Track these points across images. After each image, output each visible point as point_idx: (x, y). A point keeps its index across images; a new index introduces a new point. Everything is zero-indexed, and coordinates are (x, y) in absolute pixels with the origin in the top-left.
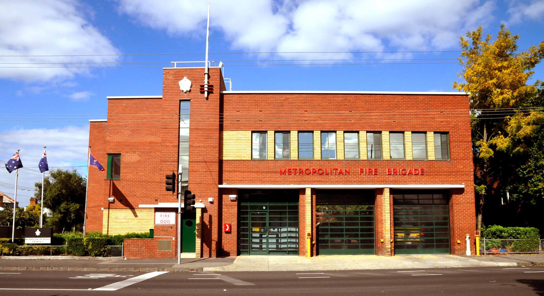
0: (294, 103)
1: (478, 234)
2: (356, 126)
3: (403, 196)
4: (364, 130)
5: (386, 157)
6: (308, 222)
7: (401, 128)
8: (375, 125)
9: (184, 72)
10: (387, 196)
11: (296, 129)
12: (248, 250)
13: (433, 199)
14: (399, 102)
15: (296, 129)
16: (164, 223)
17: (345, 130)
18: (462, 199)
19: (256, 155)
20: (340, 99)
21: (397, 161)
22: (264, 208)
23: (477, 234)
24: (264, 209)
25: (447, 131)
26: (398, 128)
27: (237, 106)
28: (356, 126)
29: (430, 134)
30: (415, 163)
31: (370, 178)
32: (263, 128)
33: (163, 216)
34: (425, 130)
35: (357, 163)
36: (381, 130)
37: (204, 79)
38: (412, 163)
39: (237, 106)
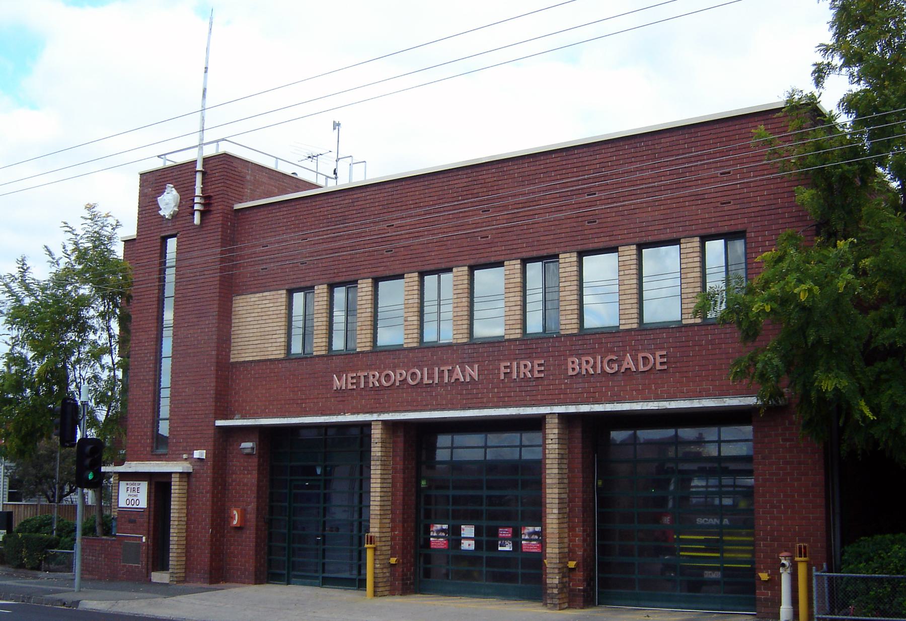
0: (368, 209)
1: (805, 556)
2: (496, 249)
3: (676, 432)
4: (514, 256)
5: (568, 327)
6: (554, 496)
7: (607, 239)
8: (542, 238)
9: (168, 175)
10: (552, 436)
11: (369, 275)
12: (285, 572)
13: (719, 442)
14: (606, 164)
15: (369, 275)
16: (132, 506)
17: (472, 262)
18: (783, 440)
19: (297, 348)
20: (463, 181)
21: (593, 337)
22: (319, 471)
23: (800, 556)
24: (320, 475)
25: (740, 228)
26: (600, 240)
27: (743, 211)
28: (496, 249)
29: (689, 245)
30: (643, 337)
31: (526, 389)
32: (307, 279)
33: (129, 489)
34: (675, 236)
35: (496, 349)
36: (557, 251)
37: (195, 185)
38: (636, 338)
39: (743, 211)
